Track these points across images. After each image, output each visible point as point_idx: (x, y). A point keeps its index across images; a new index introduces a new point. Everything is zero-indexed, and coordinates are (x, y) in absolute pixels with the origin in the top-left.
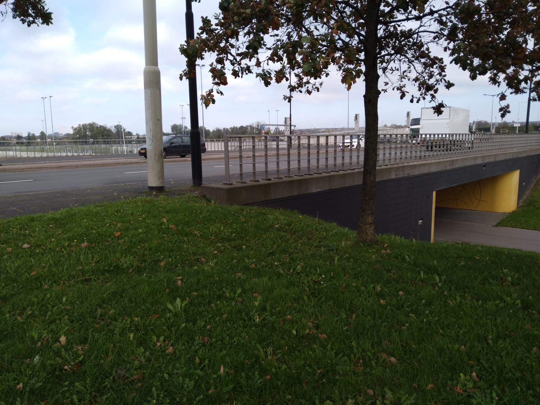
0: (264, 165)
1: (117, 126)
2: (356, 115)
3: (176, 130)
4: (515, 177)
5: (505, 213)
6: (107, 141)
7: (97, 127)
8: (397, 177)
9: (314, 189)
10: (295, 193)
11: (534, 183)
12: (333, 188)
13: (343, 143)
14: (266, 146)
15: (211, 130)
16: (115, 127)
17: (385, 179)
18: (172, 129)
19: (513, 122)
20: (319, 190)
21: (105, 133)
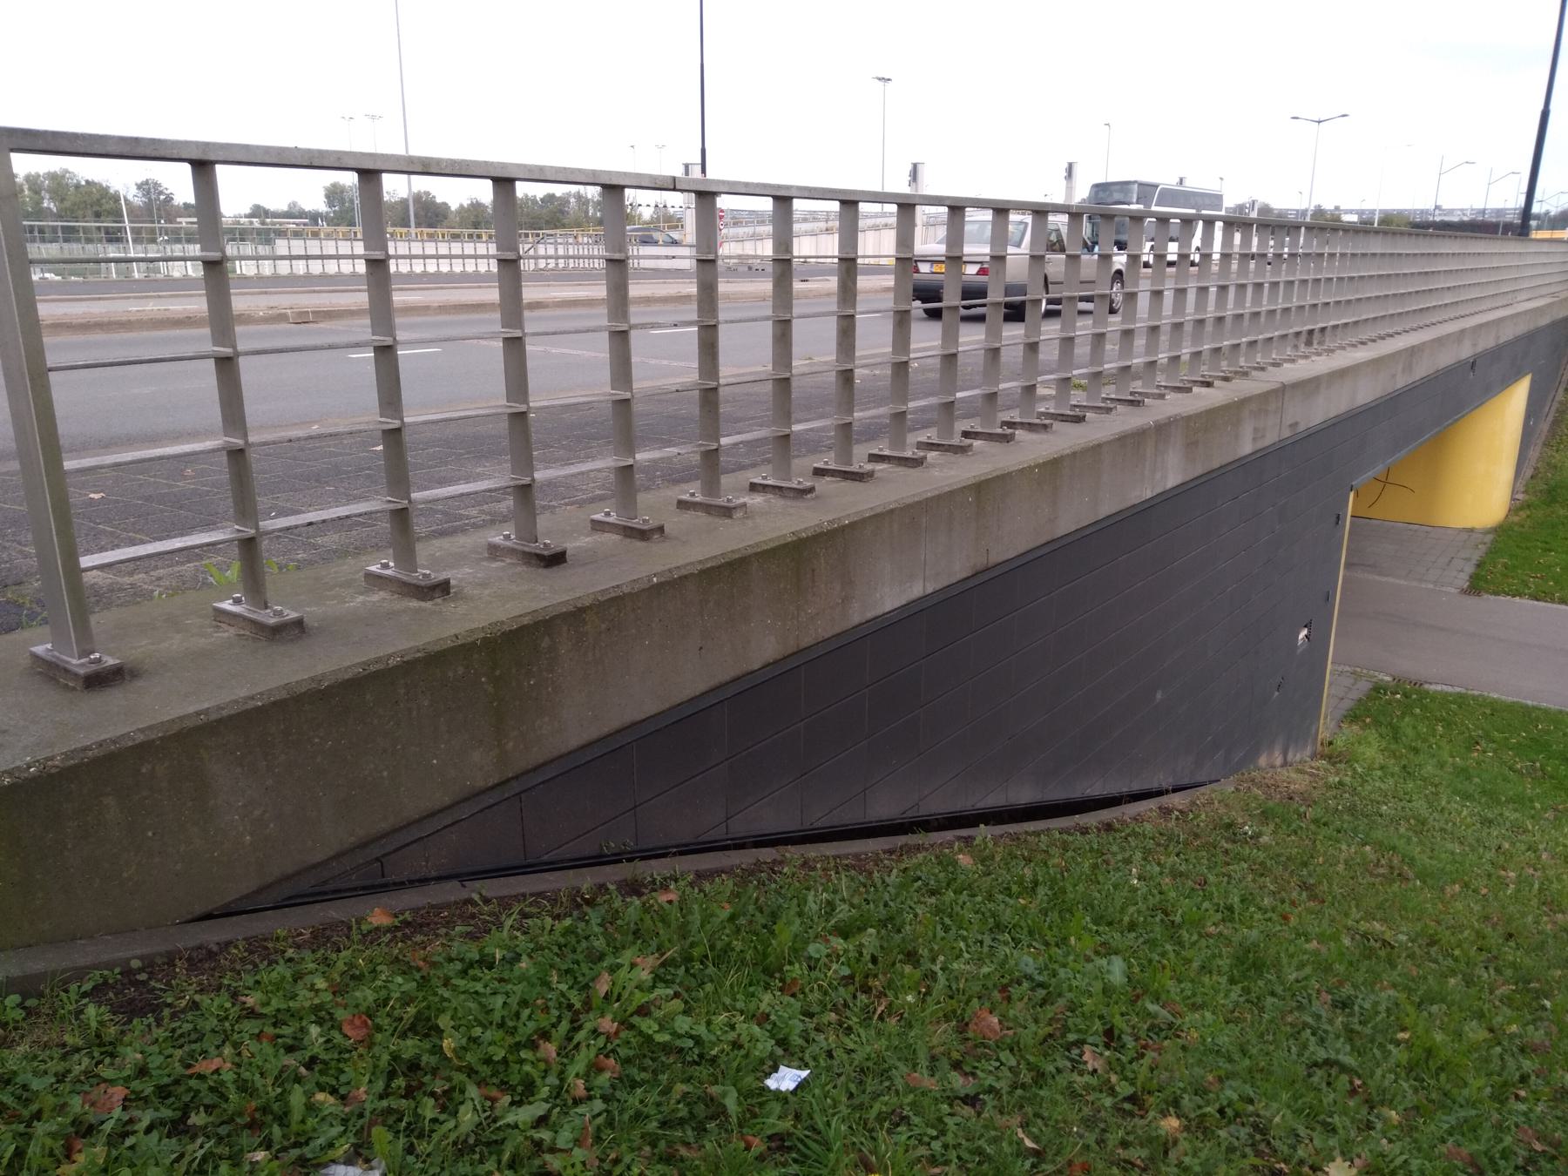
0: (599, 350)
1: (147, 182)
2: (915, 166)
3: (342, 201)
4: (1517, 398)
5: (1472, 530)
6: (41, 230)
7: (78, 186)
8: (1260, 445)
9: (889, 591)
10: (763, 644)
11: (1550, 418)
12: (996, 558)
13: (398, 257)
14: (378, 266)
15: (454, 207)
16: (139, 187)
17: (1216, 465)
18: (327, 197)
19: (1337, 208)
20: (917, 590)
21: (107, 207)
